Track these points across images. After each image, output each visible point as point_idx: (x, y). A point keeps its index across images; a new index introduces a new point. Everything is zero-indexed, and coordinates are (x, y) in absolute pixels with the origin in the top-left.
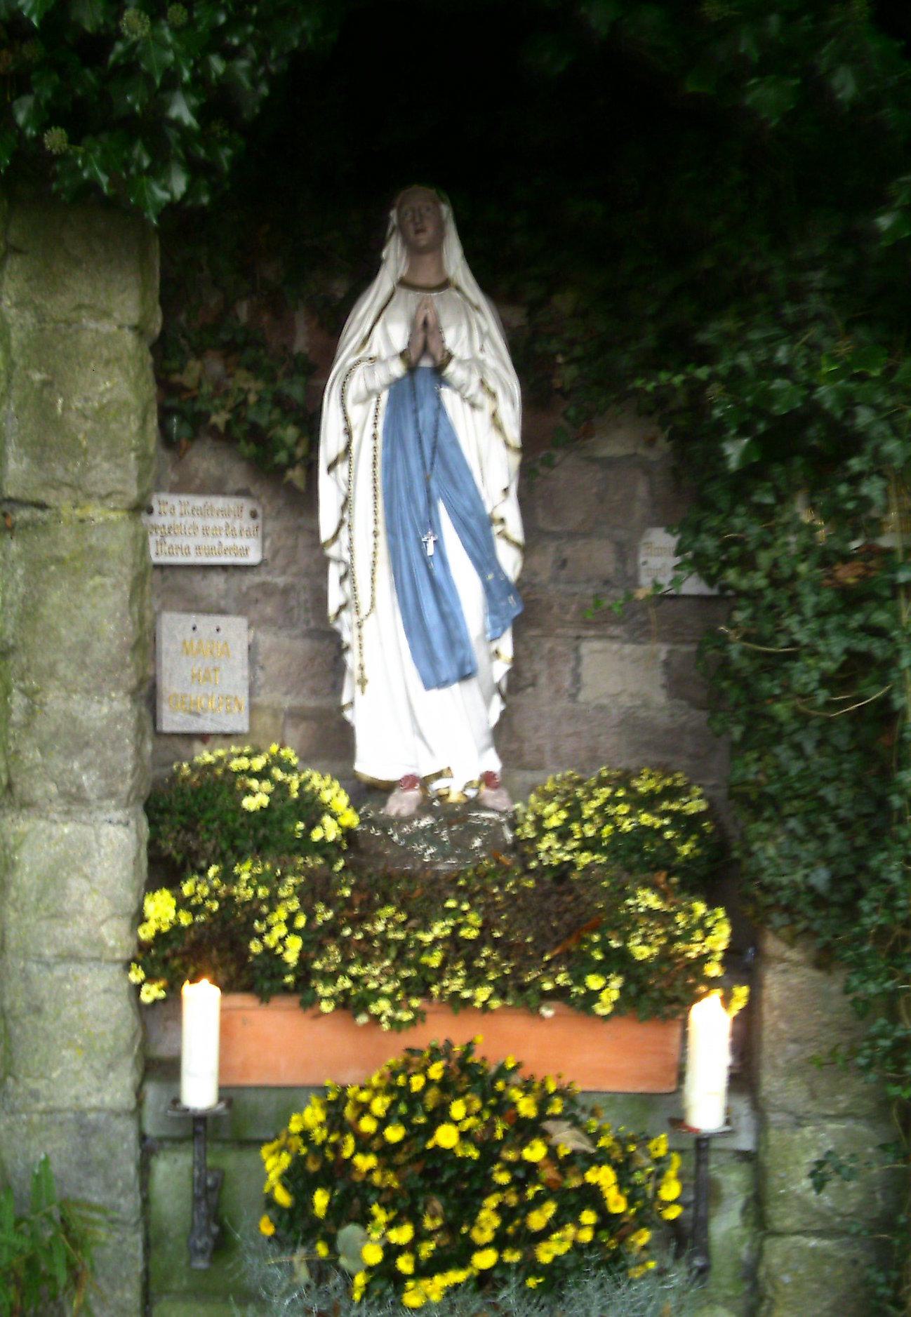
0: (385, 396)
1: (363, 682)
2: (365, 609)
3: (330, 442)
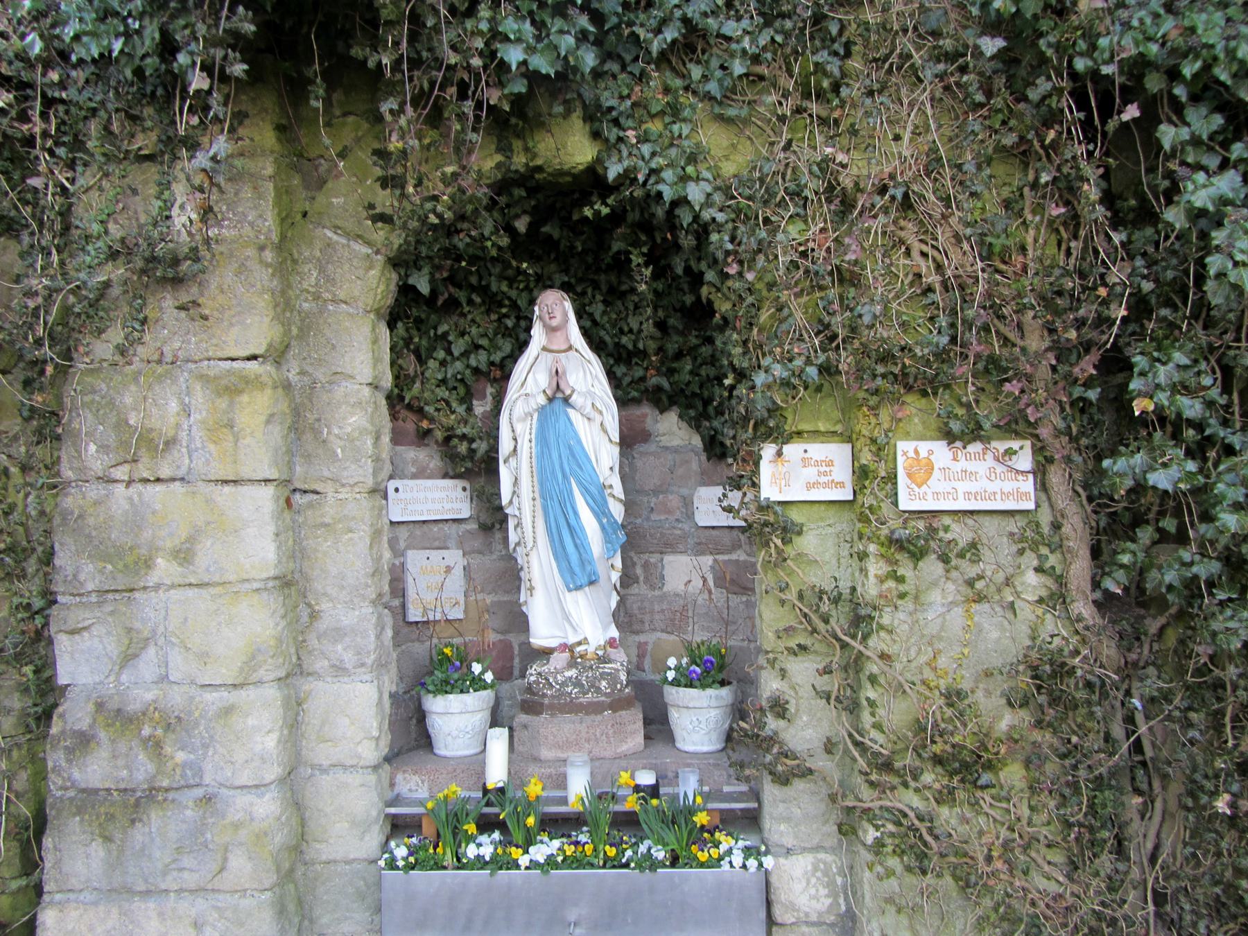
0: (536, 416)
1: (531, 589)
2: (530, 544)
3: (505, 446)
